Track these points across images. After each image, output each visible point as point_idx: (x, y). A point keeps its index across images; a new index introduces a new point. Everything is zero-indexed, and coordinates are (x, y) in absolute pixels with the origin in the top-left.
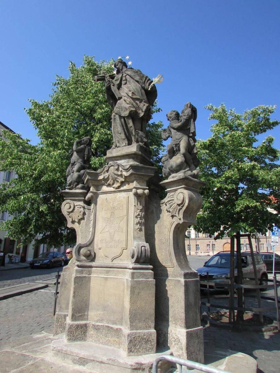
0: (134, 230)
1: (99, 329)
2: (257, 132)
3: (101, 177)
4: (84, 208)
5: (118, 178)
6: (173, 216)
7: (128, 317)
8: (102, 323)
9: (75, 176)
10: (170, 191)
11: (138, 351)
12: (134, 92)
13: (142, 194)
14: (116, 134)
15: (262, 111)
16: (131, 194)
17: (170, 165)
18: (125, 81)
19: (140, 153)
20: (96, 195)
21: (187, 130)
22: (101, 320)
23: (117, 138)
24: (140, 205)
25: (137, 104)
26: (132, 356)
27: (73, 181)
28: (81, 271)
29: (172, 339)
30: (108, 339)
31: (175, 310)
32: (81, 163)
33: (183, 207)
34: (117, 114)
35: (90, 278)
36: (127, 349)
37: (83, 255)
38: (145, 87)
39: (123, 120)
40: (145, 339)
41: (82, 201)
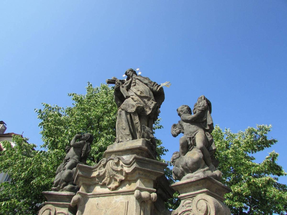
2: (254, 150)
3: (95, 174)
5: (117, 175)
10: (184, 198)
13: (147, 198)
14: (120, 129)
15: (259, 129)
16: (132, 199)
17: (184, 162)
18: (134, 84)
19: (146, 148)
20: (85, 198)
21: (203, 122)
23: (120, 133)
25: (144, 102)
34: (123, 110)
38: (154, 89)
39: (129, 116)
41: (66, 207)
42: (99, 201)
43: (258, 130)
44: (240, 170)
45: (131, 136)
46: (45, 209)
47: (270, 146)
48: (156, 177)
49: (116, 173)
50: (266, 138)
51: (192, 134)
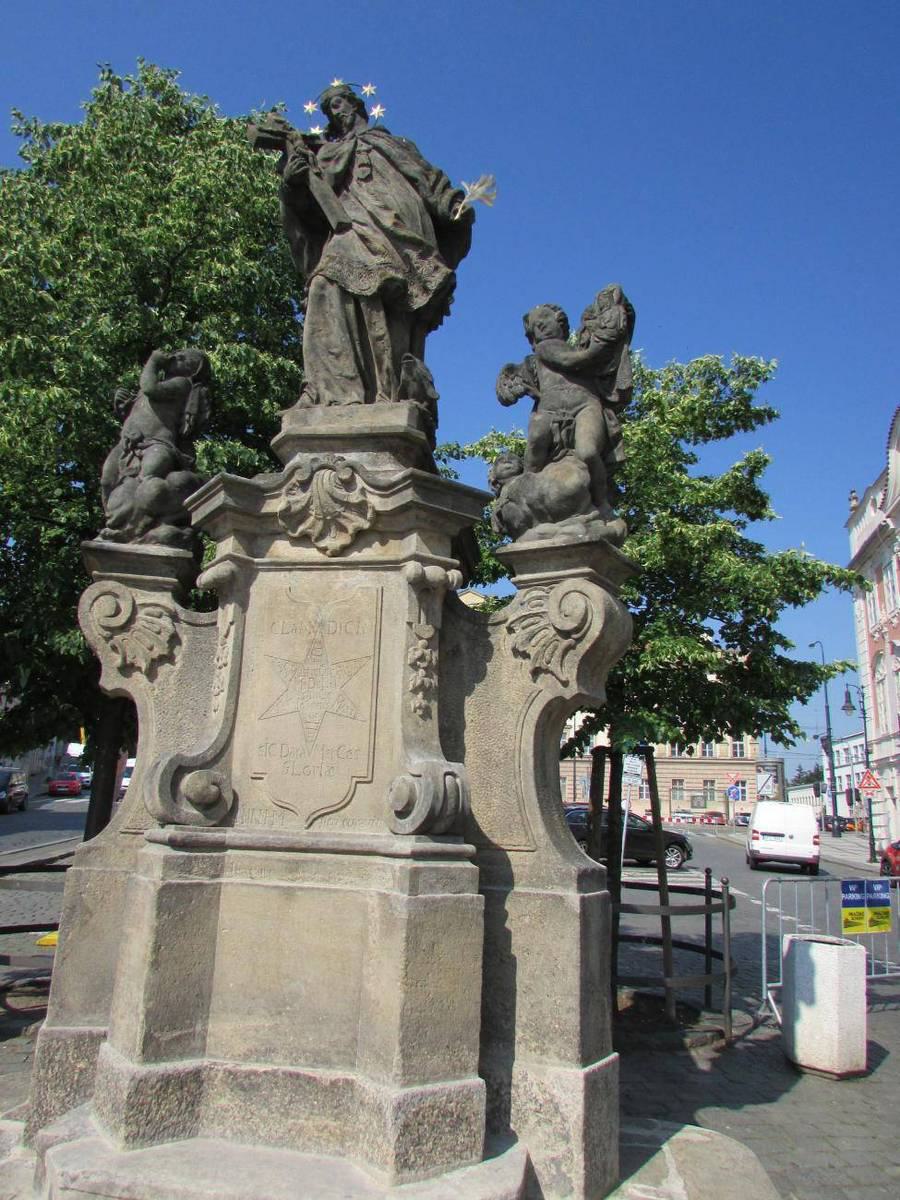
0: (406, 713)
1: (255, 1087)
3: (275, 506)
4: (174, 617)
5: (345, 514)
6: (536, 673)
7: (398, 1038)
8: (266, 1062)
9: (145, 491)
11: (429, 1161)
12: (401, 216)
21: (603, 378)
22: (268, 1052)
24: (428, 623)
25: (406, 259)
26: (410, 1182)
27: (135, 512)
28: (184, 864)
29: (528, 1105)
30: (295, 1124)
31: (540, 1003)
32: (169, 446)
33: (579, 640)
34: (331, 281)
35: (217, 889)
36: (391, 1159)
37: (189, 799)
39: (351, 307)
40: (452, 1114)
41: (165, 590)
42: (292, 582)
43: (733, 373)
44: (649, 494)
45: (361, 383)
46: (97, 593)
47: (753, 429)
48: (458, 529)
49: (342, 509)
50: (750, 400)
51: (567, 412)
